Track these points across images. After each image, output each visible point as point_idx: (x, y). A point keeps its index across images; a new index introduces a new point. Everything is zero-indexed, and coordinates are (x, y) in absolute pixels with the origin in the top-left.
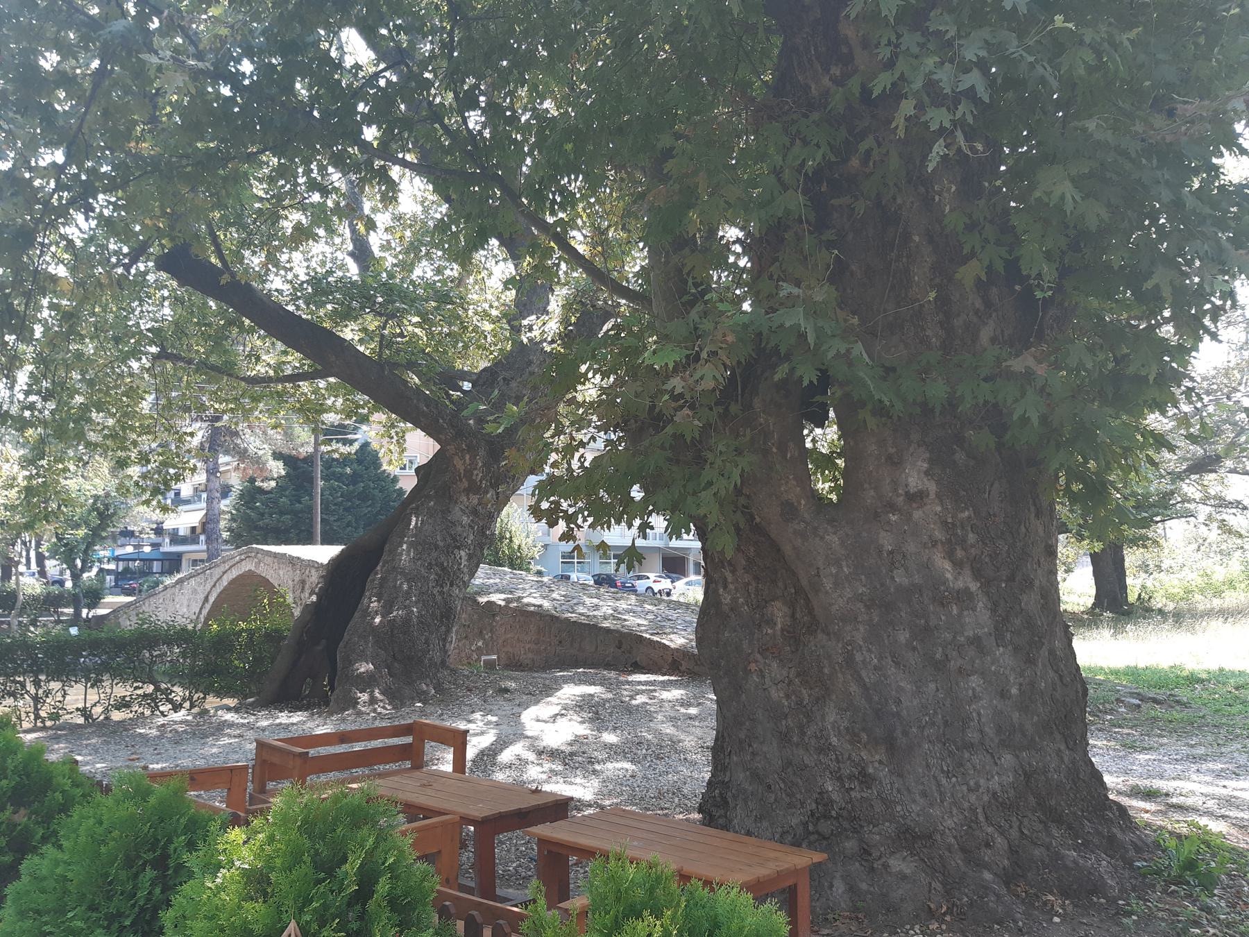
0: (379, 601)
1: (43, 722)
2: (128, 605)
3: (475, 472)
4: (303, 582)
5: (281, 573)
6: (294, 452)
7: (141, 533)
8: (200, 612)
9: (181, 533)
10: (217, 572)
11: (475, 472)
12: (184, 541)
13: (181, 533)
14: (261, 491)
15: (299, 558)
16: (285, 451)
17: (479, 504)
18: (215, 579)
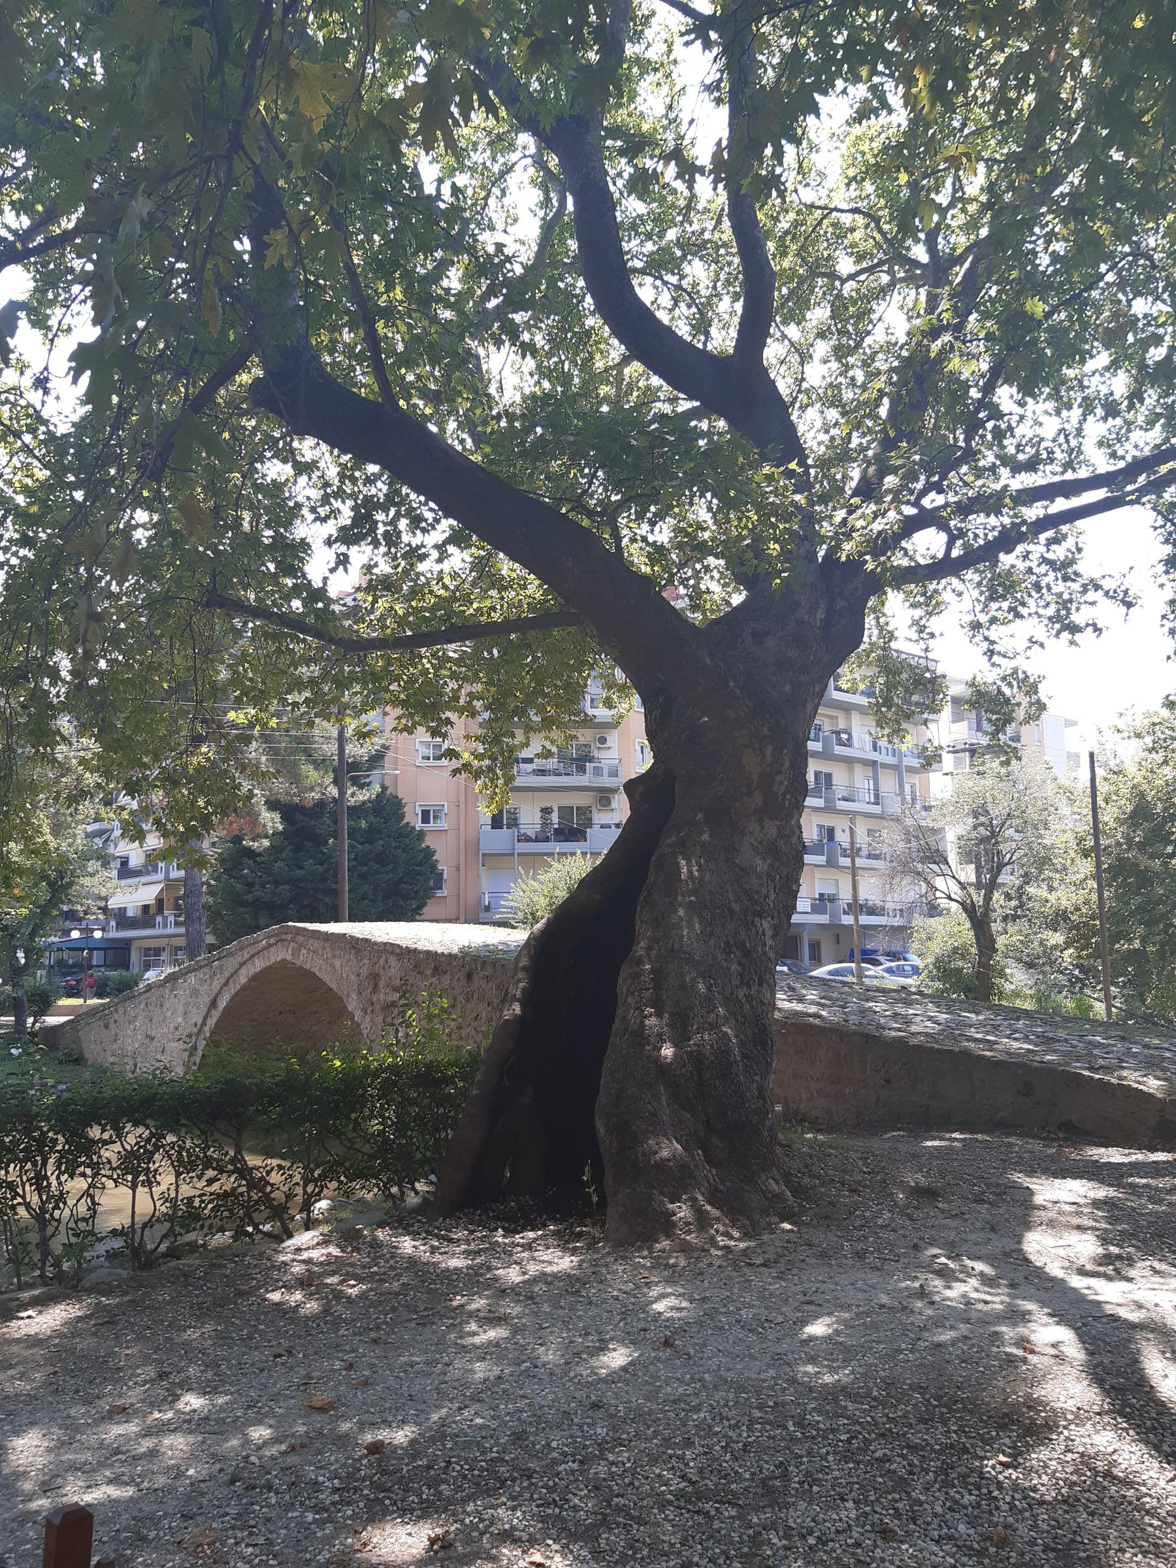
0: (659, 1015)
1: (57, 1264)
2: (93, 1012)
3: (778, 778)
4: (375, 977)
5: (337, 963)
6: (297, 800)
7: (86, 913)
8: (204, 1024)
9: (130, 913)
10: (231, 963)
11: (778, 778)
12: (132, 923)
13: (130, 913)
14: (250, 853)
15: (367, 940)
16: (283, 798)
17: (780, 836)
18: (226, 974)
